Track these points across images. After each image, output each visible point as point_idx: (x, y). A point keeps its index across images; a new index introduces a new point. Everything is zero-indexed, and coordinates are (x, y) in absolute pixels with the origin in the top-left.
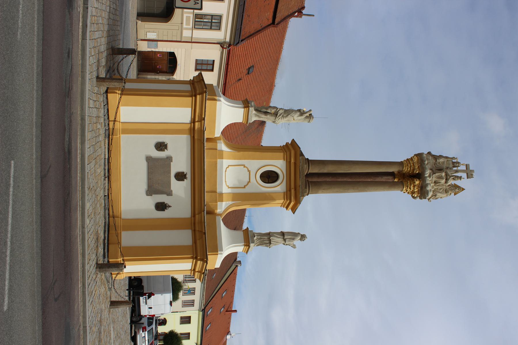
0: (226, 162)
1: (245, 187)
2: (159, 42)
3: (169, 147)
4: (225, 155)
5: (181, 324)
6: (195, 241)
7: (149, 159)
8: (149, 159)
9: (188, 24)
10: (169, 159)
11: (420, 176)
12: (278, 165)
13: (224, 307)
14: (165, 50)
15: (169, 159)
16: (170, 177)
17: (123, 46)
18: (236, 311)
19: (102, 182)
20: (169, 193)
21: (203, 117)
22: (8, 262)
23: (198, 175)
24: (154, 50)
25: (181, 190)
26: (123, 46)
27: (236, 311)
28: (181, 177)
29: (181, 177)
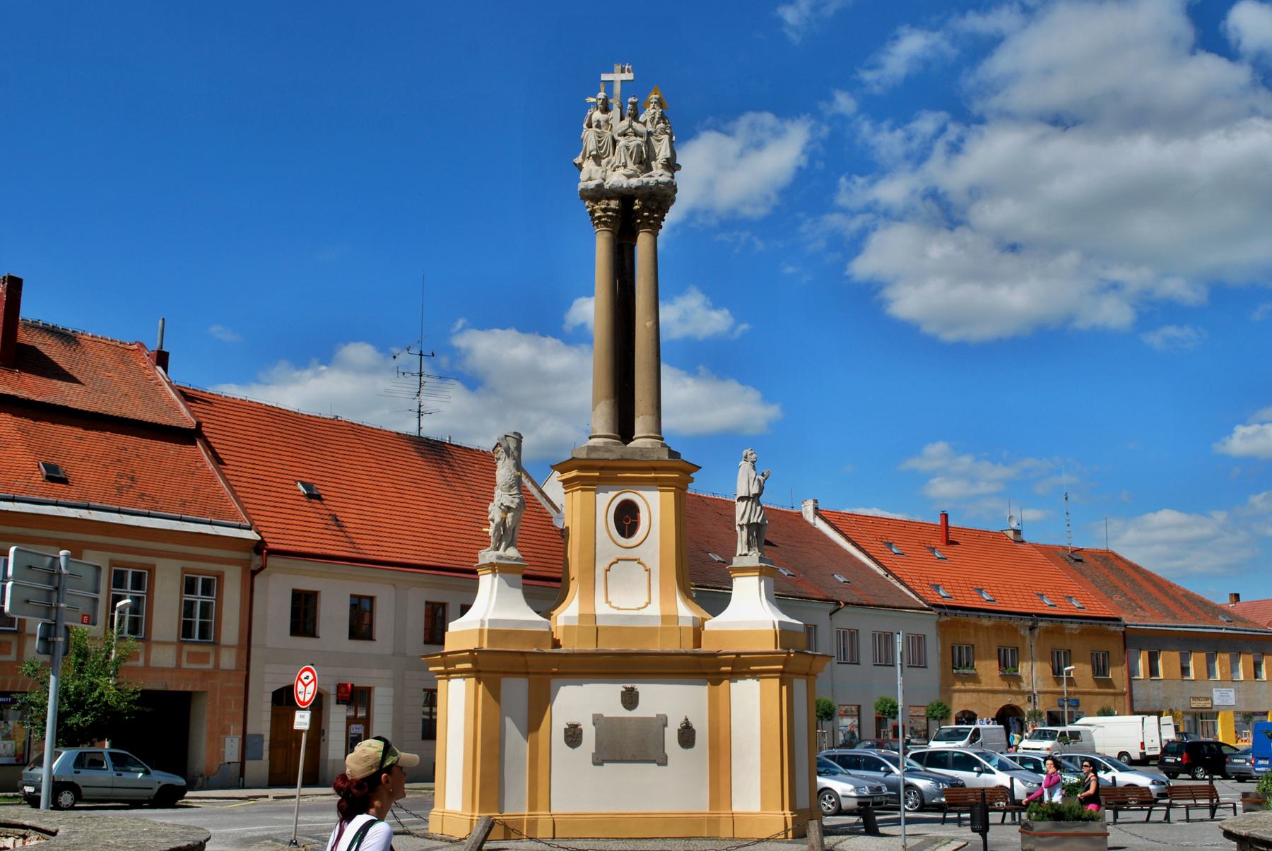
0: (601, 608)
1: (648, 570)
2: (249, 731)
3: (574, 721)
4: (588, 611)
5: (427, 603)
6: (755, 675)
7: (598, 761)
8: (598, 761)
9: (204, 658)
10: (597, 720)
11: (626, 197)
12: (606, 501)
13: (933, 549)
14: (267, 716)
15: (597, 720)
16: (630, 719)
17: (959, 691)
18: (945, 516)
19: (668, 842)
20: (663, 722)
21: (784, 688)
22: (899, 649)
23: (627, 665)
24: (266, 745)
25: (666, 701)
26: (959, 691)
27: (945, 516)
28: (630, 699)
29: (630, 699)
